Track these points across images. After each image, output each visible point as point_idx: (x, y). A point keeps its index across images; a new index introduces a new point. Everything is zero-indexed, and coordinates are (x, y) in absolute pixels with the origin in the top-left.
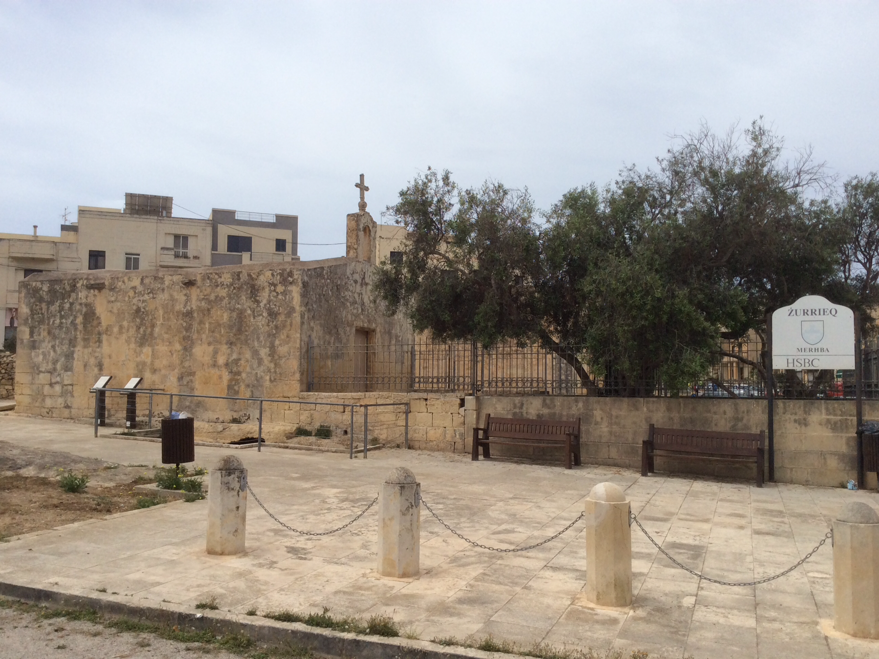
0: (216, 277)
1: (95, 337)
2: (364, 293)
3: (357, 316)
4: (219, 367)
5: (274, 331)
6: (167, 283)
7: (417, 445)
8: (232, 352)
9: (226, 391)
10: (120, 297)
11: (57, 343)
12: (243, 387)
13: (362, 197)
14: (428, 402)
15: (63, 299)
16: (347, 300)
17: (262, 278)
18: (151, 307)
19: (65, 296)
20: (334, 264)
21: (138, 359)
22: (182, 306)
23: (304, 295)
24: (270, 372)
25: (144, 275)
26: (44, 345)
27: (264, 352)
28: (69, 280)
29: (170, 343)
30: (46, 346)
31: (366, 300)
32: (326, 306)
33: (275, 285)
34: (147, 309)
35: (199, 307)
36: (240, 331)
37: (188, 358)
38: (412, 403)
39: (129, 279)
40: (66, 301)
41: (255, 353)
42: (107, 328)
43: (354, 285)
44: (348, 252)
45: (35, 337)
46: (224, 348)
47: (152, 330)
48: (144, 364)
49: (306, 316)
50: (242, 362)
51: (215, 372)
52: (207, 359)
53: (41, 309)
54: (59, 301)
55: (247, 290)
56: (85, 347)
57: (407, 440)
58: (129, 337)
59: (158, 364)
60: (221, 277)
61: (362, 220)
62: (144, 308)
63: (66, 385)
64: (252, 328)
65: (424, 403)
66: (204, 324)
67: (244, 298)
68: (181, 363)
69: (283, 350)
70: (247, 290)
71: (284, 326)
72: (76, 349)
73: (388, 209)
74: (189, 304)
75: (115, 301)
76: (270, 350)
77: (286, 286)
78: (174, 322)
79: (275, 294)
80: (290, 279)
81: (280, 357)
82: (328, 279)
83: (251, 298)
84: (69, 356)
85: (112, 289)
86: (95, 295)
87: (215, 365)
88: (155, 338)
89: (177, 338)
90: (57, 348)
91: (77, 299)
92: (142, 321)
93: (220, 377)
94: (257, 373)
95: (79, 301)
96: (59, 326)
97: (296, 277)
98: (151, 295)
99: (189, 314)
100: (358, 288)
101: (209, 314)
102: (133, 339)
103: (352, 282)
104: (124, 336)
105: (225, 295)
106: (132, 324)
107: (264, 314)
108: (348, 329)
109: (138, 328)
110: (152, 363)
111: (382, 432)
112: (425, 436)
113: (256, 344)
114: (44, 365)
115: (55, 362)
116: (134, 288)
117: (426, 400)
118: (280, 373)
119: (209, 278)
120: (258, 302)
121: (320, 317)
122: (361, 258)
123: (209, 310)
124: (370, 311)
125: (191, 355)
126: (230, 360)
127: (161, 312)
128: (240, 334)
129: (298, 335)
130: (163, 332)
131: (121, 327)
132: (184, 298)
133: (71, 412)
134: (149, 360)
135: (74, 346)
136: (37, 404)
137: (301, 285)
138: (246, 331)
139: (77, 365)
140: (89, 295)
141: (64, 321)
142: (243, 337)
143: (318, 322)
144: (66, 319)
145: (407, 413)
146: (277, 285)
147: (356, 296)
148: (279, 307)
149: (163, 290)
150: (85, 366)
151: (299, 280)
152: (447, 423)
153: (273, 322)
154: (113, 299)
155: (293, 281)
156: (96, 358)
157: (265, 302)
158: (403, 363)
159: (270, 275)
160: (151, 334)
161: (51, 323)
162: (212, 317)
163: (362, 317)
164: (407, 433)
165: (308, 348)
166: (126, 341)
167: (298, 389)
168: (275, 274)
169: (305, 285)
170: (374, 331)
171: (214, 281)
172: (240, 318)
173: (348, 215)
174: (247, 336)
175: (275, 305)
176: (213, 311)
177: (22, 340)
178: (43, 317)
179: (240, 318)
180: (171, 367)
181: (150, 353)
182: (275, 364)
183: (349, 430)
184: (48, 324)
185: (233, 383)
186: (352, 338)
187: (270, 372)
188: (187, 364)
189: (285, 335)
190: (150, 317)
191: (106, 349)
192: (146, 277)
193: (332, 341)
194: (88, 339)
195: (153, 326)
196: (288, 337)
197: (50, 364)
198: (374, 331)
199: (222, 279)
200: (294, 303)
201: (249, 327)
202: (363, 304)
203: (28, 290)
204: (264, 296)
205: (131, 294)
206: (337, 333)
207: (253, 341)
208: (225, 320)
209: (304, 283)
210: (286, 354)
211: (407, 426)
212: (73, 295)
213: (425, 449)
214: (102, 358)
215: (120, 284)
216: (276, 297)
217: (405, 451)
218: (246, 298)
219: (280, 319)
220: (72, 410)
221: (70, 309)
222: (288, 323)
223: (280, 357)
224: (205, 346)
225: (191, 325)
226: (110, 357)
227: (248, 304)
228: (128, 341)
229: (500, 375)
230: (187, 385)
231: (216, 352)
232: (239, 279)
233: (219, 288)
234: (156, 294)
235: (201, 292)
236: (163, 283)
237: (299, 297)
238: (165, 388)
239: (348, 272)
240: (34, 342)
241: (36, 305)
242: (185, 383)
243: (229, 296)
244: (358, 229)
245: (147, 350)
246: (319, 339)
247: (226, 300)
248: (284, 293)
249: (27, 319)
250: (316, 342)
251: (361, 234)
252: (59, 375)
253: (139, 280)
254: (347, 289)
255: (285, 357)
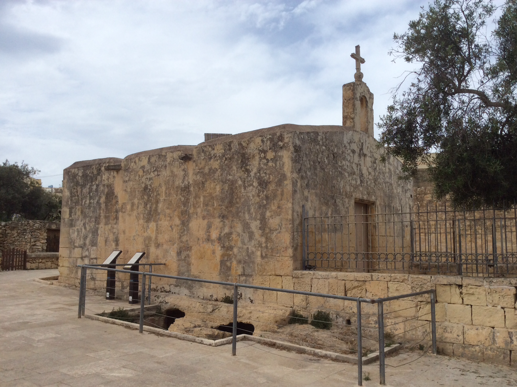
0: (210, 149)
1: (113, 214)
2: (362, 163)
3: (356, 187)
4: (212, 241)
5: (265, 202)
6: (168, 160)
7: (449, 348)
8: (224, 226)
9: (219, 266)
10: (132, 177)
11: (87, 221)
12: (235, 263)
13: (358, 68)
14: (464, 290)
15: (92, 182)
16: (345, 170)
17: (252, 145)
18: (156, 184)
19: (93, 179)
20: (330, 130)
21: (146, 234)
22: (181, 181)
23: (296, 160)
24: (262, 247)
25: (151, 154)
26: (78, 223)
27: (255, 225)
28: (96, 165)
29: (171, 217)
30: (79, 224)
31: (365, 171)
32: (321, 174)
33: (265, 152)
34: (153, 186)
35: (194, 181)
36: (231, 203)
37: (186, 232)
38: (440, 290)
39: (139, 160)
40: (94, 183)
41: (246, 226)
42: (122, 206)
43: (352, 155)
44: (344, 122)
45: (72, 217)
46: (217, 222)
47: (157, 206)
48: (149, 238)
49: (299, 184)
50: (234, 236)
51: (208, 246)
52: (202, 234)
53: (77, 192)
54: (89, 184)
55: (238, 160)
56: (106, 224)
57: (434, 339)
58: (138, 214)
59: (161, 239)
60: (214, 149)
61: (359, 89)
62: (151, 186)
63: (92, 259)
64: (243, 200)
65: (458, 291)
66: (200, 198)
67: (234, 168)
68: (180, 238)
69: (274, 222)
70: (238, 160)
71: (275, 196)
72: (100, 226)
73: (395, 37)
74: (186, 178)
75: (129, 180)
76: (261, 223)
77: (276, 152)
78: (175, 198)
79: (265, 161)
80: (280, 143)
81: (271, 231)
82: (323, 145)
83: (241, 168)
84: (95, 232)
85: (127, 170)
86: (114, 177)
87: (209, 239)
88: (159, 214)
89: (176, 213)
90: (87, 226)
91: (101, 181)
92: (148, 198)
93: (214, 252)
94: (248, 248)
95: (103, 183)
96: (89, 206)
97: (286, 140)
98: (156, 173)
99: (186, 189)
100: (356, 159)
101: (203, 187)
102: (142, 216)
103: (349, 151)
104: (135, 213)
105: (217, 167)
106: (141, 201)
107: (254, 184)
108: (347, 200)
109: (146, 204)
110: (156, 239)
111: (397, 326)
112: (461, 337)
113: (247, 216)
114: (78, 241)
115: (85, 238)
116: (143, 167)
117: (460, 286)
118: (271, 248)
119: (203, 150)
120: (248, 171)
121: (315, 186)
122: (358, 127)
123: (203, 183)
124: (369, 183)
125: (188, 230)
126: (222, 234)
127: (164, 188)
128: (231, 207)
129: (290, 205)
130: (165, 207)
131: (133, 204)
132: (182, 173)
133: (95, 283)
134: (153, 236)
135: (99, 224)
136: (73, 276)
137: (292, 149)
138: (237, 203)
139: (100, 240)
140: (110, 177)
141: (92, 201)
142: (234, 210)
143: (314, 191)
144: (93, 200)
145: (434, 302)
146: (267, 151)
147: (354, 166)
148: (269, 175)
149: (166, 167)
150: (106, 241)
151: (290, 144)
152: (497, 320)
153: (263, 192)
154: (127, 179)
155: (284, 145)
156: (114, 233)
157: (255, 170)
158: (403, 237)
159: (260, 142)
160: (156, 210)
161: (83, 204)
162: (206, 191)
163: (361, 189)
164: (434, 332)
165: (301, 220)
166: (136, 217)
167: (291, 268)
168: (265, 139)
169: (297, 149)
170: (373, 203)
171: (208, 153)
172: (232, 189)
173: (344, 86)
174: (238, 208)
175: (265, 173)
176: (207, 185)
177: (64, 219)
178: (79, 199)
179: (232, 189)
180: (171, 241)
181: (155, 228)
182: (267, 238)
183: (353, 319)
184: (82, 205)
185: (226, 258)
186: (352, 211)
187: (262, 247)
188: (184, 239)
189: (276, 205)
190: (155, 194)
191: (121, 225)
192: (153, 156)
193: (330, 213)
194: (109, 216)
195: (157, 202)
196: (279, 207)
197: (82, 239)
198: (373, 203)
199: (215, 151)
200: (285, 169)
201: (240, 199)
202: (361, 175)
203: (69, 176)
204: (254, 165)
205: (141, 173)
206: (335, 204)
207: (244, 213)
208: (217, 193)
209: (295, 147)
210: (277, 227)
211: (433, 321)
212: (99, 178)
213: (462, 355)
214: (118, 233)
215: (132, 164)
216: (266, 164)
217: (433, 358)
218: (237, 168)
219: (271, 188)
220: (96, 282)
221: (97, 190)
222: (279, 192)
223: (271, 230)
224: (200, 220)
225: (188, 199)
226: (124, 232)
227: (238, 174)
228: (138, 218)
229: (423, 249)
230: (184, 260)
231: (209, 226)
232: (230, 150)
233: (212, 160)
234: (160, 171)
235: (196, 166)
236: (165, 161)
237: (290, 163)
238: (167, 263)
239: (346, 141)
240: (72, 220)
241: (74, 189)
242: (183, 258)
243: (221, 167)
244: (354, 98)
245: (152, 225)
246: (315, 211)
247: (219, 173)
248: (275, 160)
249: (68, 201)
250: (311, 213)
251: (358, 103)
252: (88, 249)
253: (147, 159)
254: (344, 159)
255: (276, 230)
